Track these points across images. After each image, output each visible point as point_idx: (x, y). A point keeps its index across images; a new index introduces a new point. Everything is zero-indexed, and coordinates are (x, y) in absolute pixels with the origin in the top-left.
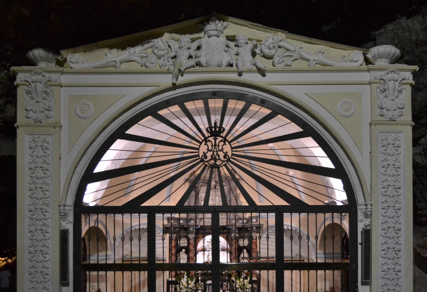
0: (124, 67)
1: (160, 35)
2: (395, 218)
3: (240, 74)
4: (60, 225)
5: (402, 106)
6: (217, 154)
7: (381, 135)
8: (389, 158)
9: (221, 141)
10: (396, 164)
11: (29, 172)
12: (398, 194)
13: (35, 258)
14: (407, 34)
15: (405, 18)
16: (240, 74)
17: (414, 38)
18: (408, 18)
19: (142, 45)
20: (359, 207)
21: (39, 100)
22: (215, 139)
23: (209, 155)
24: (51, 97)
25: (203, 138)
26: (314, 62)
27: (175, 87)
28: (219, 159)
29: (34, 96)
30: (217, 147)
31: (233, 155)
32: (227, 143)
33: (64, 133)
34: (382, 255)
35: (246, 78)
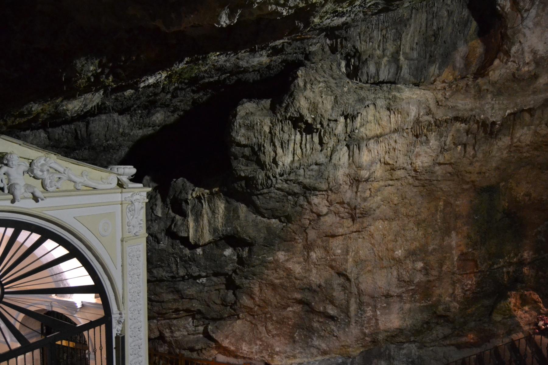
14: (116, 126)
16: (13, 201)
17: (121, 130)
20: (113, 316)
35: (20, 205)
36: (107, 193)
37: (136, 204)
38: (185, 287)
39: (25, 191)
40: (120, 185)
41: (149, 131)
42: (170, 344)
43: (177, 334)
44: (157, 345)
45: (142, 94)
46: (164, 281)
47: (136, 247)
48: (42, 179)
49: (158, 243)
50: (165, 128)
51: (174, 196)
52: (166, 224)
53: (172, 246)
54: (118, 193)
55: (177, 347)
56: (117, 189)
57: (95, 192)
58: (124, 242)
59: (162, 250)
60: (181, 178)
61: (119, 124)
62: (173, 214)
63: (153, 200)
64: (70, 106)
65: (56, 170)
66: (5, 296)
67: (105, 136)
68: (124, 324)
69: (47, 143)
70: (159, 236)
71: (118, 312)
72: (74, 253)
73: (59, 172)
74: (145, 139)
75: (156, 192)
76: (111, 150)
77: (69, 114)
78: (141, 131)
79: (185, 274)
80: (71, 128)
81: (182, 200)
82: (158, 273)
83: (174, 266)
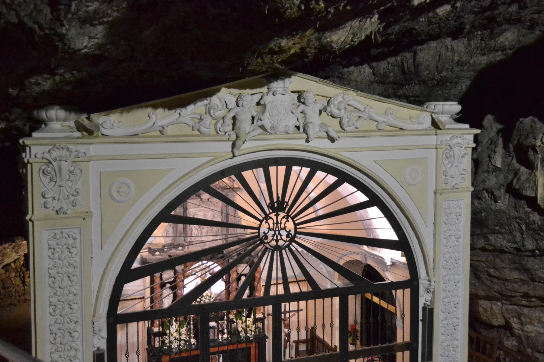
1: (218, 90)
3: (307, 141)
6: (279, 233)
9: (283, 217)
11: (48, 281)
16: (307, 141)
17: (456, 58)
18: (454, 39)
19: (195, 104)
20: (420, 281)
22: (277, 215)
25: (264, 216)
28: (282, 239)
30: (279, 225)
32: (290, 219)
33: (95, 223)
34: (443, 331)
35: (314, 144)
36: (414, 135)
37: (456, 149)
38: (537, 266)
39: (320, 130)
40: (435, 124)
41: (499, 56)
42: (519, 338)
43: (529, 328)
44: (502, 336)
45: (462, 11)
46: (506, 252)
47: (455, 202)
48: (340, 118)
49: (496, 201)
50: (521, 53)
51: (519, 141)
52: (506, 177)
53: (515, 208)
54: (432, 134)
55: (529, 346)
56: (432, 130)
57: (401, 132)
58: (438, 195)
59: (501, 211)
60: (531, 117)
61: (453, 51)
62: (517, 166)
63: (493, 146)
64: (334, 38)
65: (356, 108)
66: (297, 235)
67: (437, 67)
68: (433, 293)
69: (372, 79)
70: (496, 193)
71: (427, 278)
72: (374, 200)
73: (359, 110)
74: (491, 68)
75: (498, 135)
76: (448, 84)
77: (335, 46)
78: (485, 57)
79: (534, 248)
80: (396, 61)
81: (528, 147)
82: (496, 241)
83: (518, 235)
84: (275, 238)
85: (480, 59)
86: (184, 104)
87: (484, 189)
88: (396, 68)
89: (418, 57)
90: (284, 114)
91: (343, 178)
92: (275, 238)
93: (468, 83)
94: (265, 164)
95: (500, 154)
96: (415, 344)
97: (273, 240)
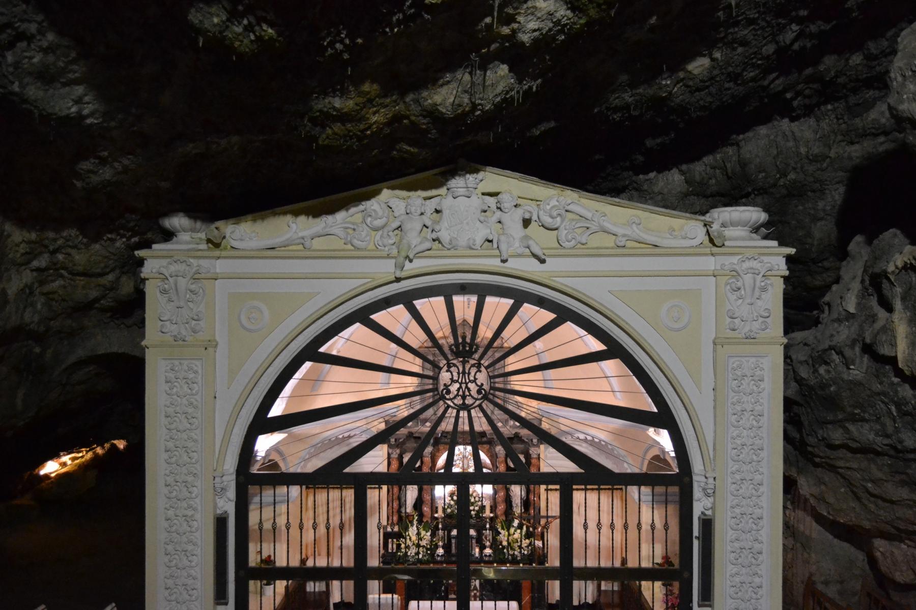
0: (317, 244)
2: (754, 498)
4: (215, 506)
5: (767, 314)
6: (467, 387)
7: (732, 360)
8: (745, 399)
10: (756, 408)
12: (759, 459)
13: (174, 562)
15: (786, 120)
20: (695, 478)
21: (182, 304)
23: (454, 388)
24: (200, 298)
26: (624, 239)
27: (398, 280)
28: (470, 395)
29: (174, 298)
31: (491, 388)
33: (221, 354)
35: (514, 265)
54: (706, 255)
57: (657, 251)
59: (856, 384)
64: (438, 99)
70: (848, 352)
78: (856, 147)
84: (461, 393)
85: (847, 148)
86: (331, 210)
87: (831, 348)
88: (718, 171)
89: (742, 151)
90: (468, 223)
91: (563, 315)
92: (461, 393)
93: (842, 189)
94: (447, 292)
95: (856, 292)
96: (686, 575)
97: (458, 395)
